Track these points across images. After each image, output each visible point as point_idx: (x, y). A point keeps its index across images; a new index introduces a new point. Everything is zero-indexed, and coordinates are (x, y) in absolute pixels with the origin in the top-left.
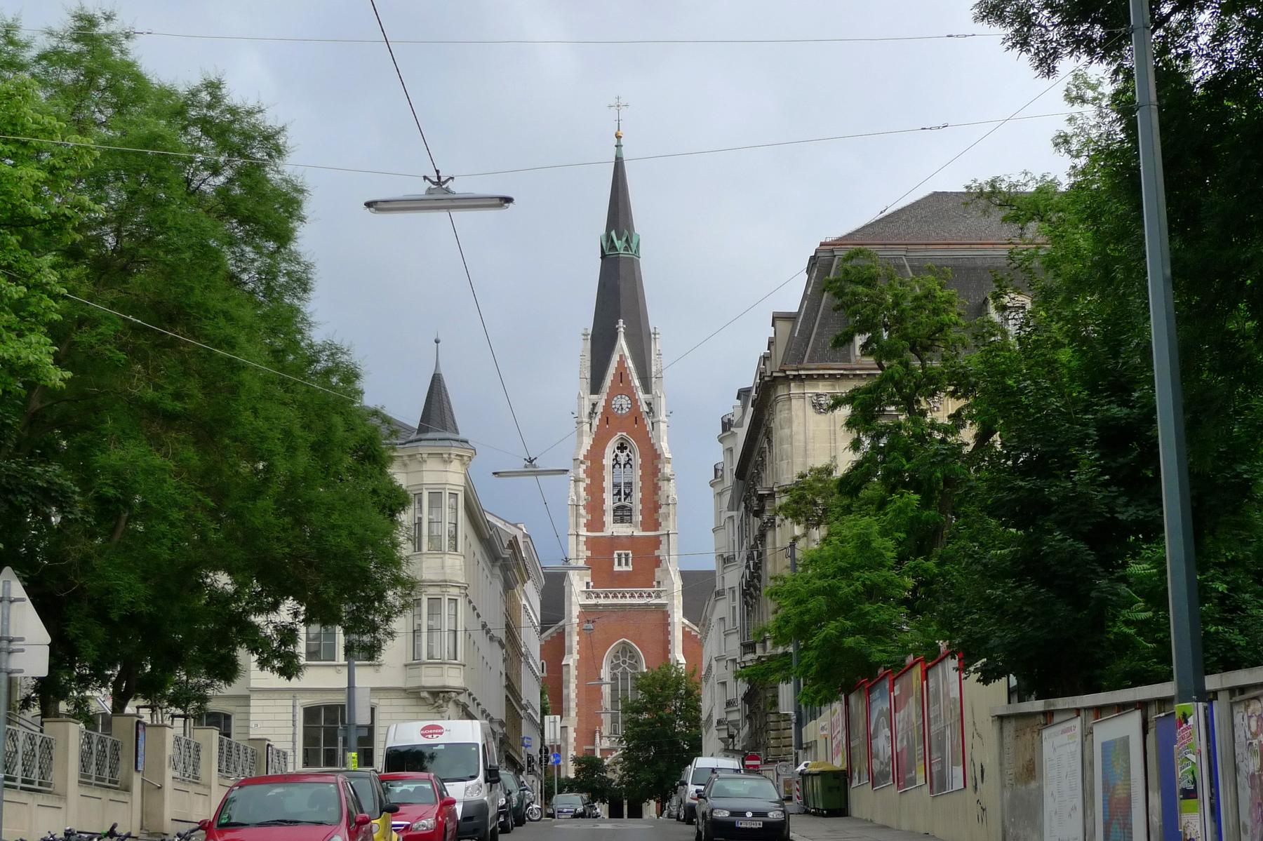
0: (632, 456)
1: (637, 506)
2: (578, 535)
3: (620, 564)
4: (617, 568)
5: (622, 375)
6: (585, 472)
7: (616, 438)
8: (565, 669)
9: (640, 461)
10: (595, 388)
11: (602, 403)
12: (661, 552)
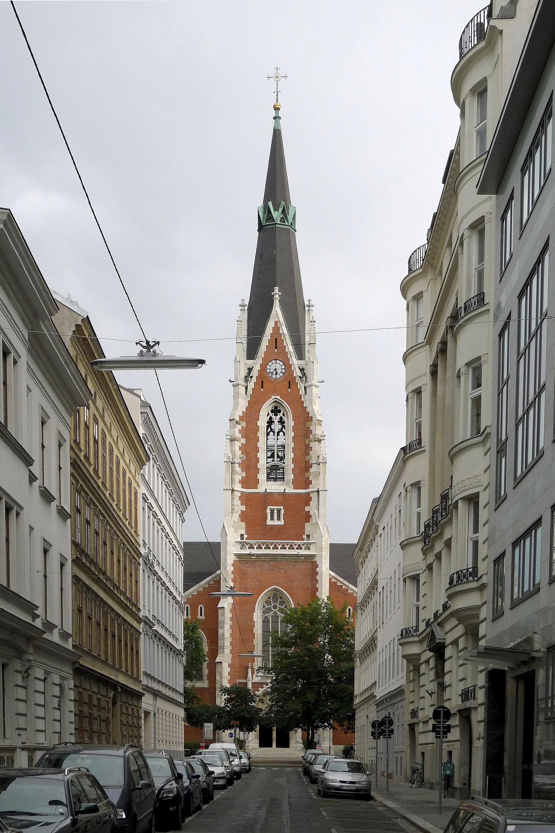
0: (285, 419)
1: (289, 464)
2: (233, 491)
3: (272, 519)
4: (269, 522)
5: (276, 341)
6: (240, 432)
8: (220, 612)
9: (292, 423)
10: (251, 354)
11: (257, 368)
12: (311, 509)
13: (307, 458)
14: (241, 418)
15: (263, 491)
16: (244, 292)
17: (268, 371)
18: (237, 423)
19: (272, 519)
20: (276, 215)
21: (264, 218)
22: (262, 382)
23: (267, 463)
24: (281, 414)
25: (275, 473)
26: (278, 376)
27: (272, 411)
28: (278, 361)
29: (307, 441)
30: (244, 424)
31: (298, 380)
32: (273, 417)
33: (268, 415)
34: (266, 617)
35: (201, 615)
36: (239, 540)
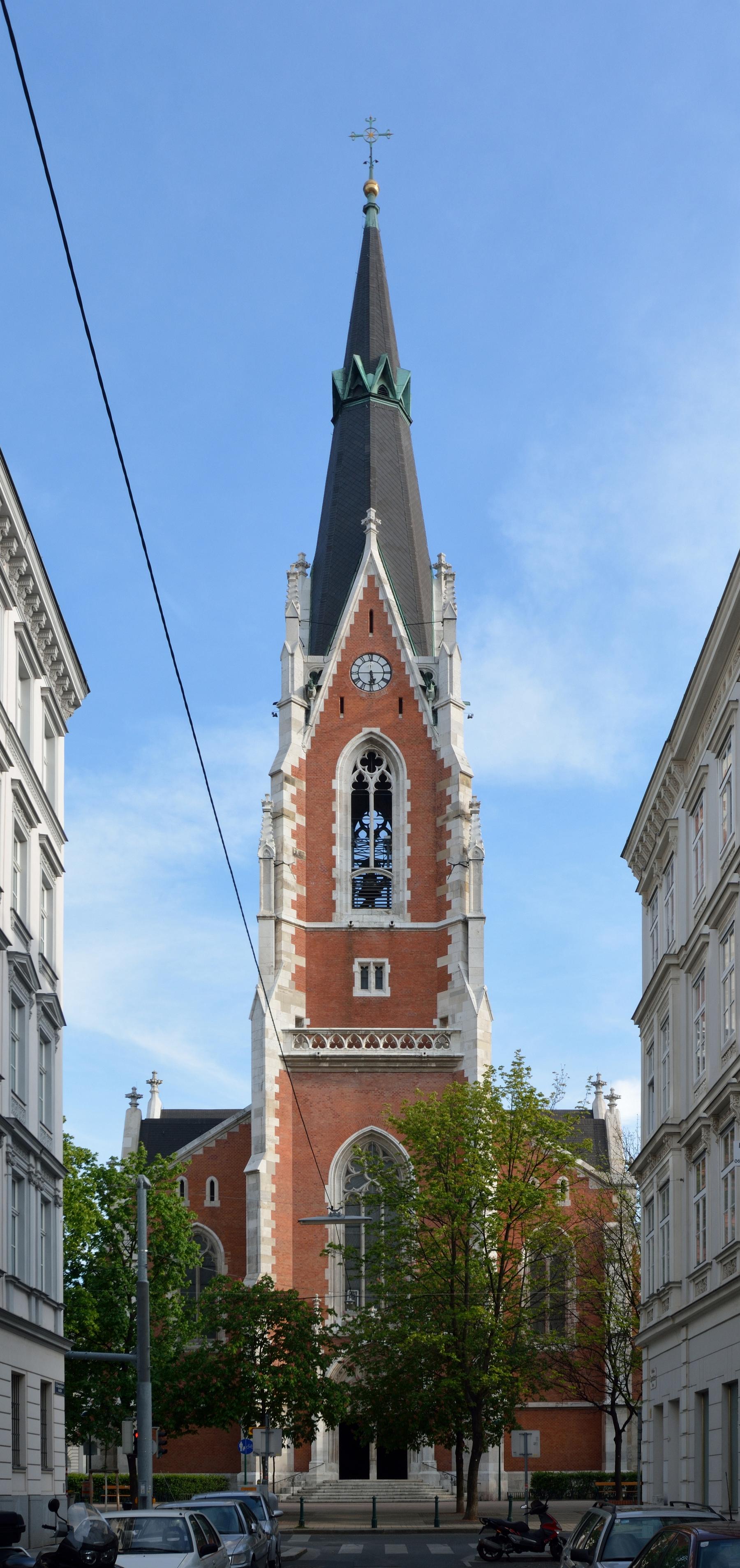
0: (391, 778)
1: (401, 871)
2: (278, 921)
3: (365, 985)
4: (358, 992)
5: (373, 616)
6: (294, 799)
7: (357, 740)
8: (250, 1181)
9: (408, 784)
10: (319, 642)
11: (331, 669)
12: (451, 961)
13: (440, 856)
14: (296, 771)
15: (345, 924)
16: (306, 542)
17: (355, 677)
18: (287, 779)
19: (365, 985)
20: (373, 382)
21: (344, 390)
22: (342, 699)
23: (353, 870)
24: (383, 767)
25: (371, 890)
26: (376, 688)
27: (363, 762)
28: (375, 658)
29: (439, 822)
30: (303, 786)
31: (418, 694)
32: (367, 774)
33: (355, 769)
34: (353, 1195)
35: (212, 1199)
36: (292, 1026)
